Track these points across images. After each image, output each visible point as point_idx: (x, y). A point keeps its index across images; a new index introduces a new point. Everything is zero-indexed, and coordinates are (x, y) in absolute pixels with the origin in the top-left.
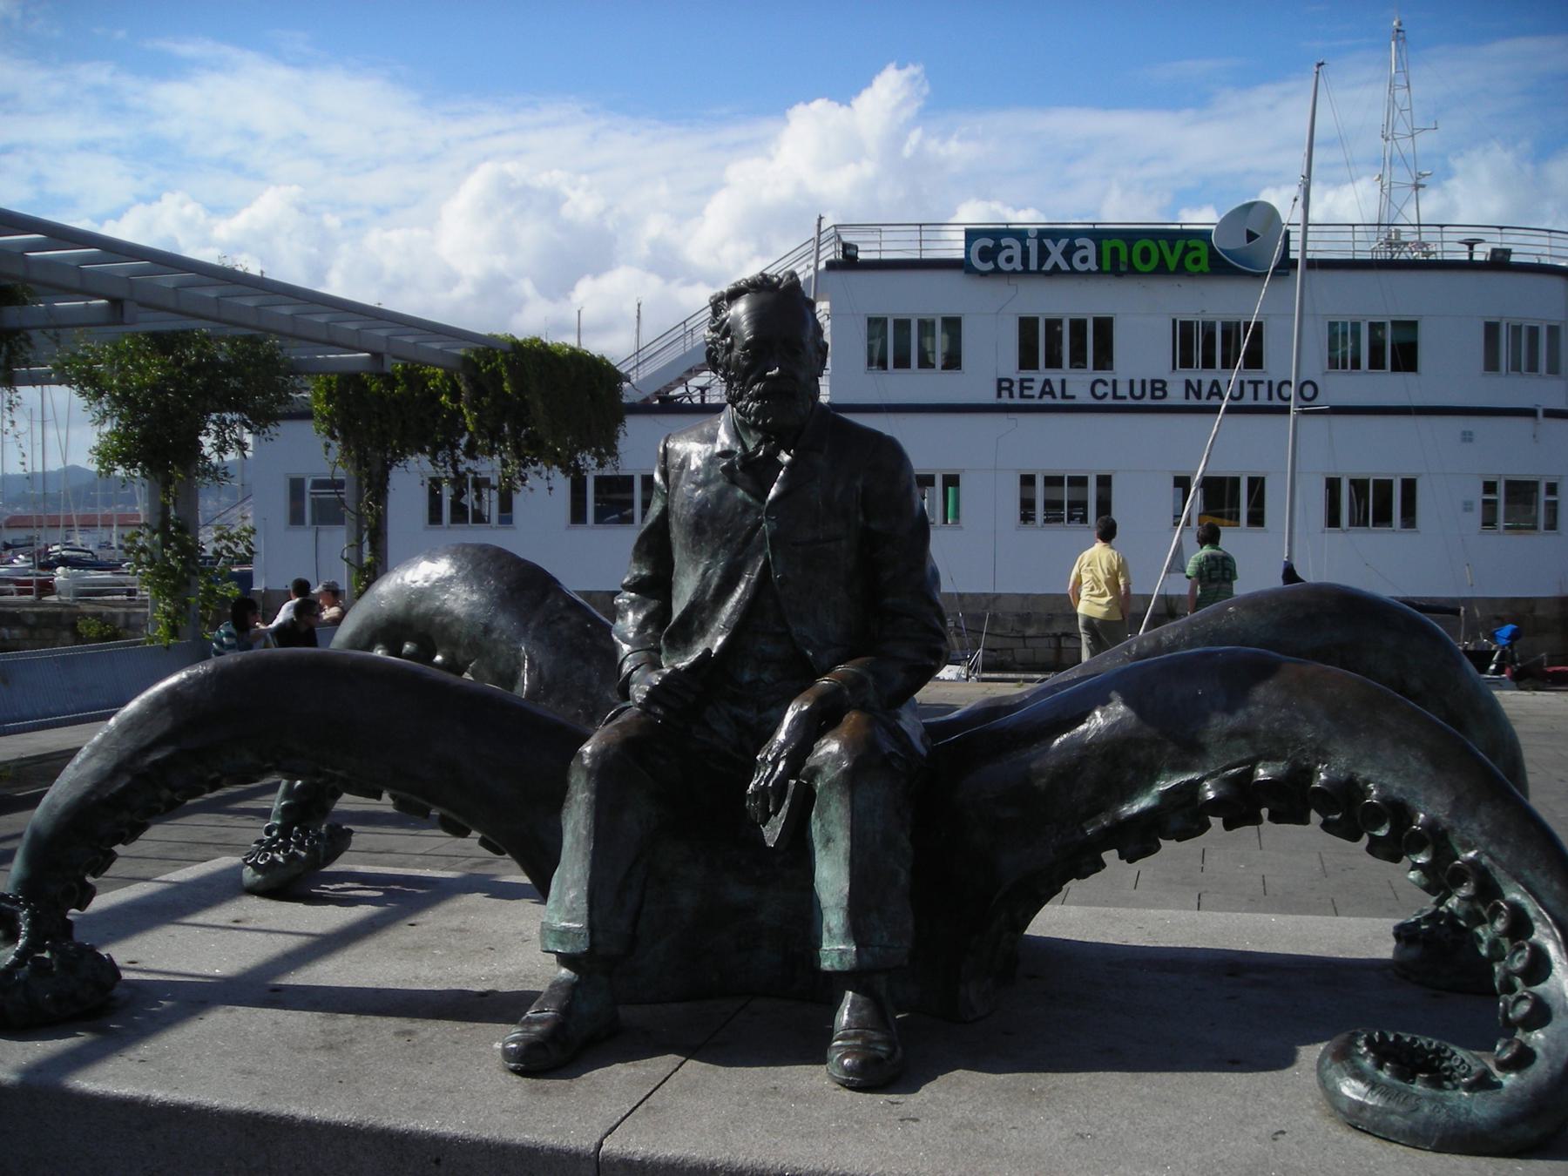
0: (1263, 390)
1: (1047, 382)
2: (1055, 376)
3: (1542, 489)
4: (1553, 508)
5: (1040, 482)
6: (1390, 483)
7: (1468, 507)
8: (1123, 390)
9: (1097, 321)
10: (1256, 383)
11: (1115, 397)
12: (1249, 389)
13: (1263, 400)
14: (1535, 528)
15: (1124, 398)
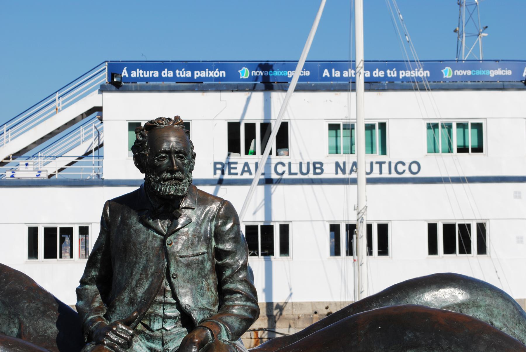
0: (385, 167)
1: (246, 164)
2: (251, 160)
8: (295, 169)
10: (381, 163)
11: (290, 173)
12: (376, 167)
13: (385, 174)
15: (296, 174)
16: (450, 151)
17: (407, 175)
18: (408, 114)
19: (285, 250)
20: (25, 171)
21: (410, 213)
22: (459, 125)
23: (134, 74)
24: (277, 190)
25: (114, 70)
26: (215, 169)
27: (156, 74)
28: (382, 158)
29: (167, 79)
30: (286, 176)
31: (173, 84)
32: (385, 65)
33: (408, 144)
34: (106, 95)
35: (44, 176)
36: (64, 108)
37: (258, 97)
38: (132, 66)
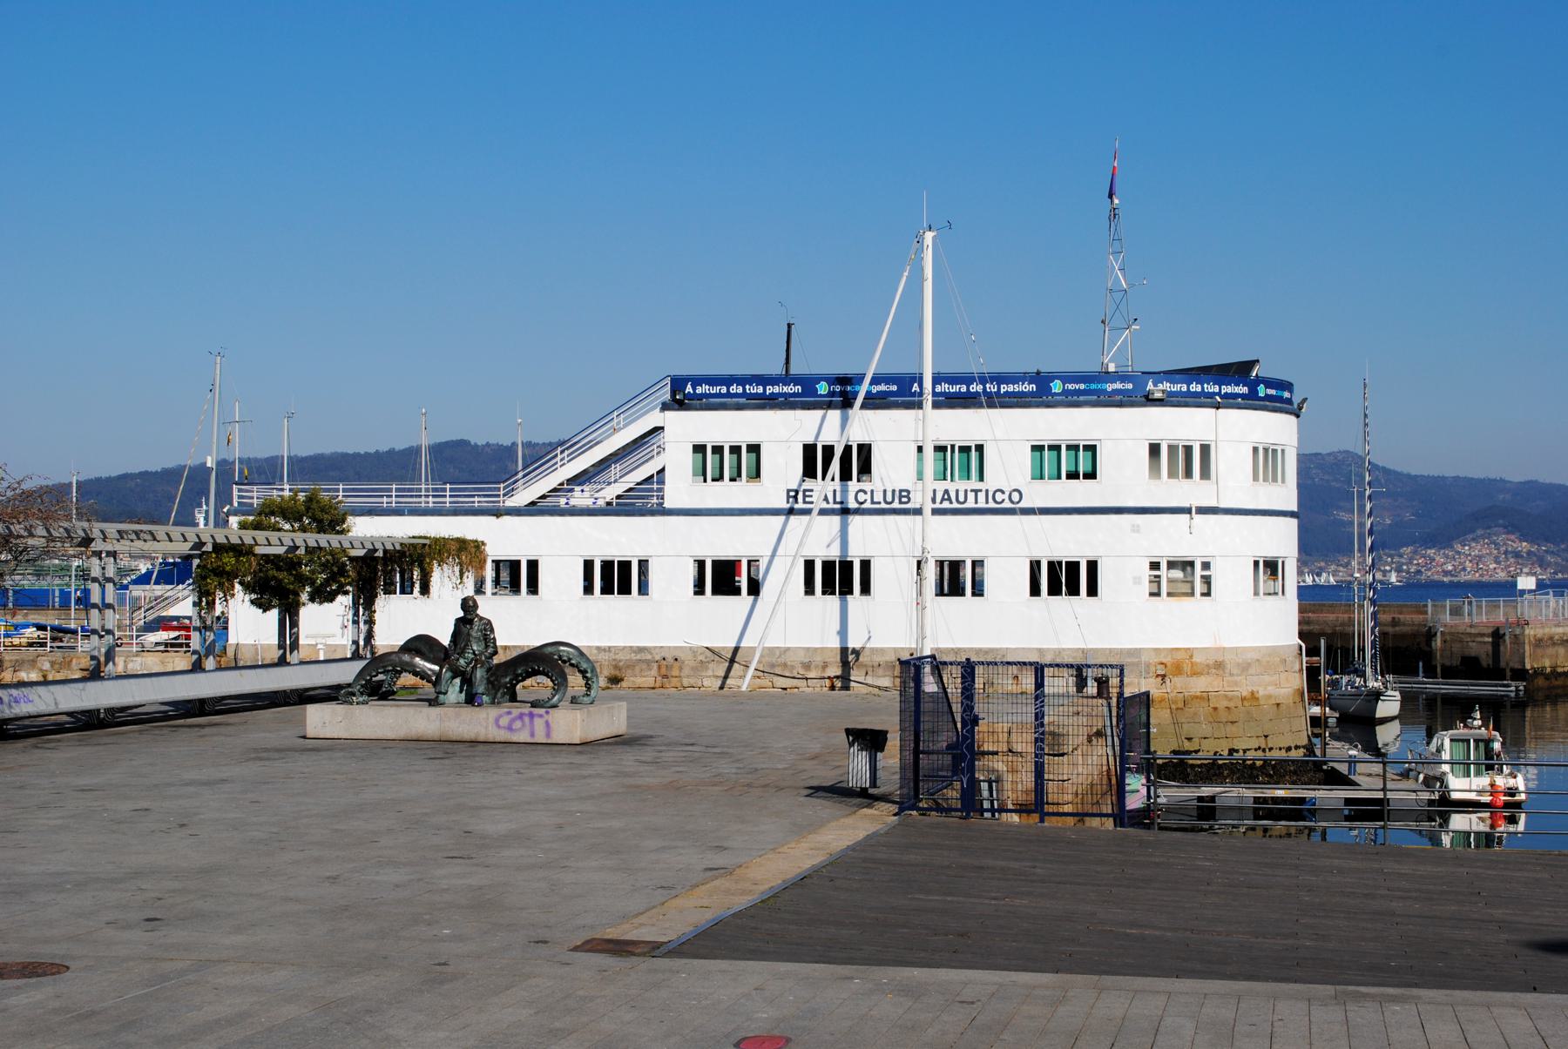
0: (981, 496)
1: (946, 492)
3: (1198, 566)
4: (1207, 581)
5: (1164, 566)
6: (629, 563)
7: (1137, 581)
8: (878, 497)
9: (860, 447)
10: (976, 492)
12: (971, 496)
13: (982, 504)
14: (1192, 594)
16: (1059, 477)
17: (1007, 505)
18: (1007, 435)
19: (866, 589)
20: (581, 498)
21: (1006, 549)
22: (1069, 447)
23: (699, 390)
24: (855, 521)
25: (678, 384)
26: (788, 497)
27: (724, 390)
28: (978, 485)
29: (736, 395)
30: (868, 505)
31: (743, 400)
32: (953, 380)
33: (1008, 467)
34: (668, 413)
35: (601, 503)
36: (625, 426)
37: (834, 415)
38: (697, 381)
